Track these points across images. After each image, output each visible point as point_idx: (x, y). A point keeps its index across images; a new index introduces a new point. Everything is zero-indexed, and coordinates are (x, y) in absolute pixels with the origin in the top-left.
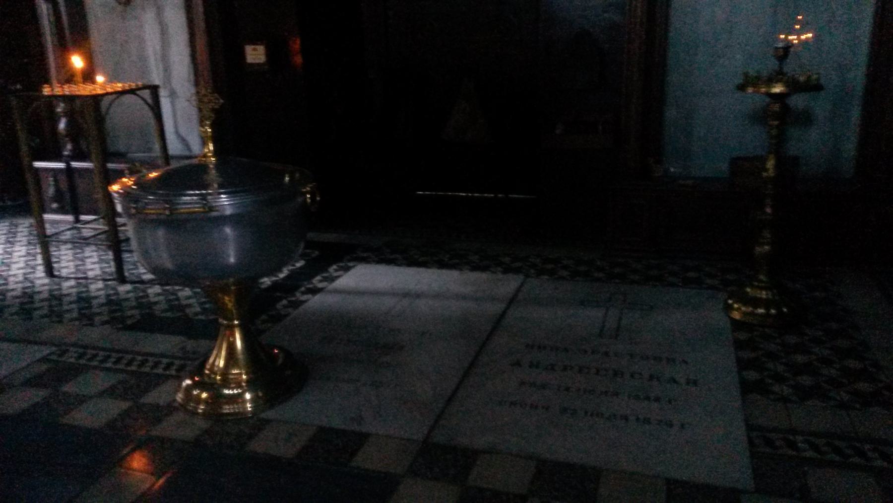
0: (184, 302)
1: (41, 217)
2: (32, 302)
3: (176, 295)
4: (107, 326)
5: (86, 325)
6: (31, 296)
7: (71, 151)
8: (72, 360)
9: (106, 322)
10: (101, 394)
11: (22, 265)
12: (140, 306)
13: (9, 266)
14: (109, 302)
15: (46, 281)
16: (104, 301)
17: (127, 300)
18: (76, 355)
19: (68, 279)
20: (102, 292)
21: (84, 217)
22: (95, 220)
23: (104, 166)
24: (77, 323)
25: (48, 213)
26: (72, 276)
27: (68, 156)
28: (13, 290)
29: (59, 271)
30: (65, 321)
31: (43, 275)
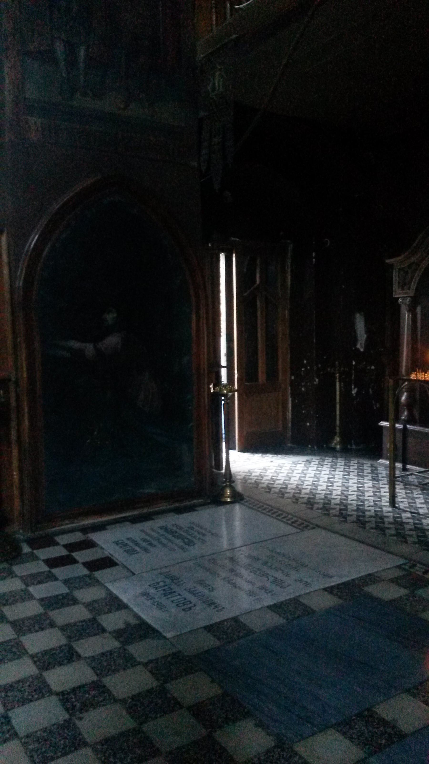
0: (385, 514)
1: (394, 464)
2: (300, 493)
3: (382, 508)
4: (355, 524)
5: (424, 549)
6: (314, 495)
7: (406, 416)
8: (420, 573)
9: (415, 543)
10: (392, 581)
11: (312, 475)
12: (358, 510)
13: (315, 476)
14: (395, 522)
15: (390, 509)
16: (339, 502)
17: (387, 517)
18: (423, 570)
19: (405, 511)
20: (355, 502)
21: (408, 466)
22: (424, 472)
23: (394, 426)
24: (304, 505)
25: (409, 464)
26: (408, 510)
27: (404, 420)
28: (291, 484)
29: (398, 504)
30: (272, 492)
31: (388, 504)
